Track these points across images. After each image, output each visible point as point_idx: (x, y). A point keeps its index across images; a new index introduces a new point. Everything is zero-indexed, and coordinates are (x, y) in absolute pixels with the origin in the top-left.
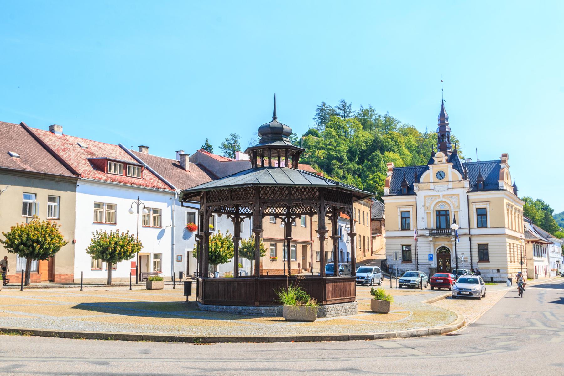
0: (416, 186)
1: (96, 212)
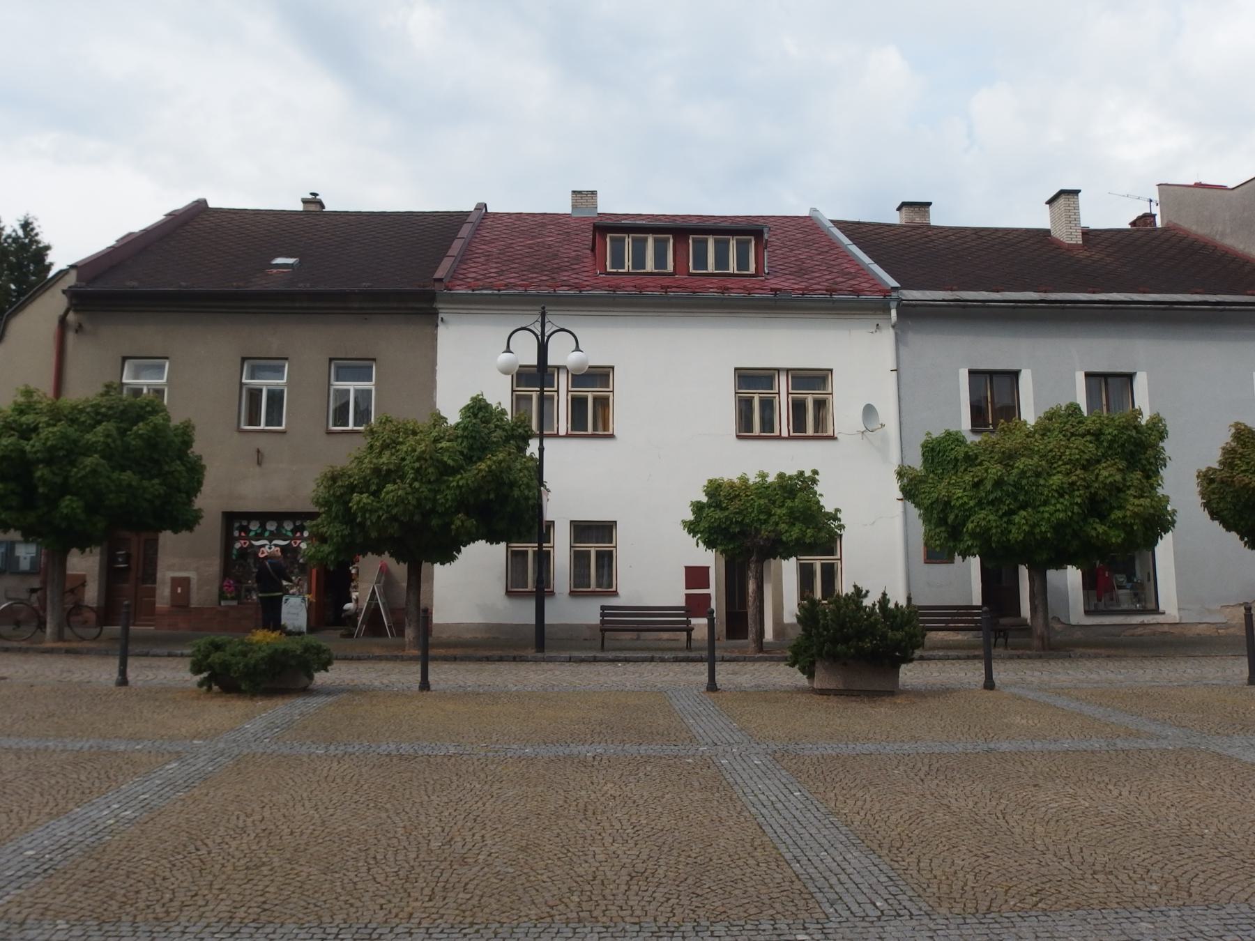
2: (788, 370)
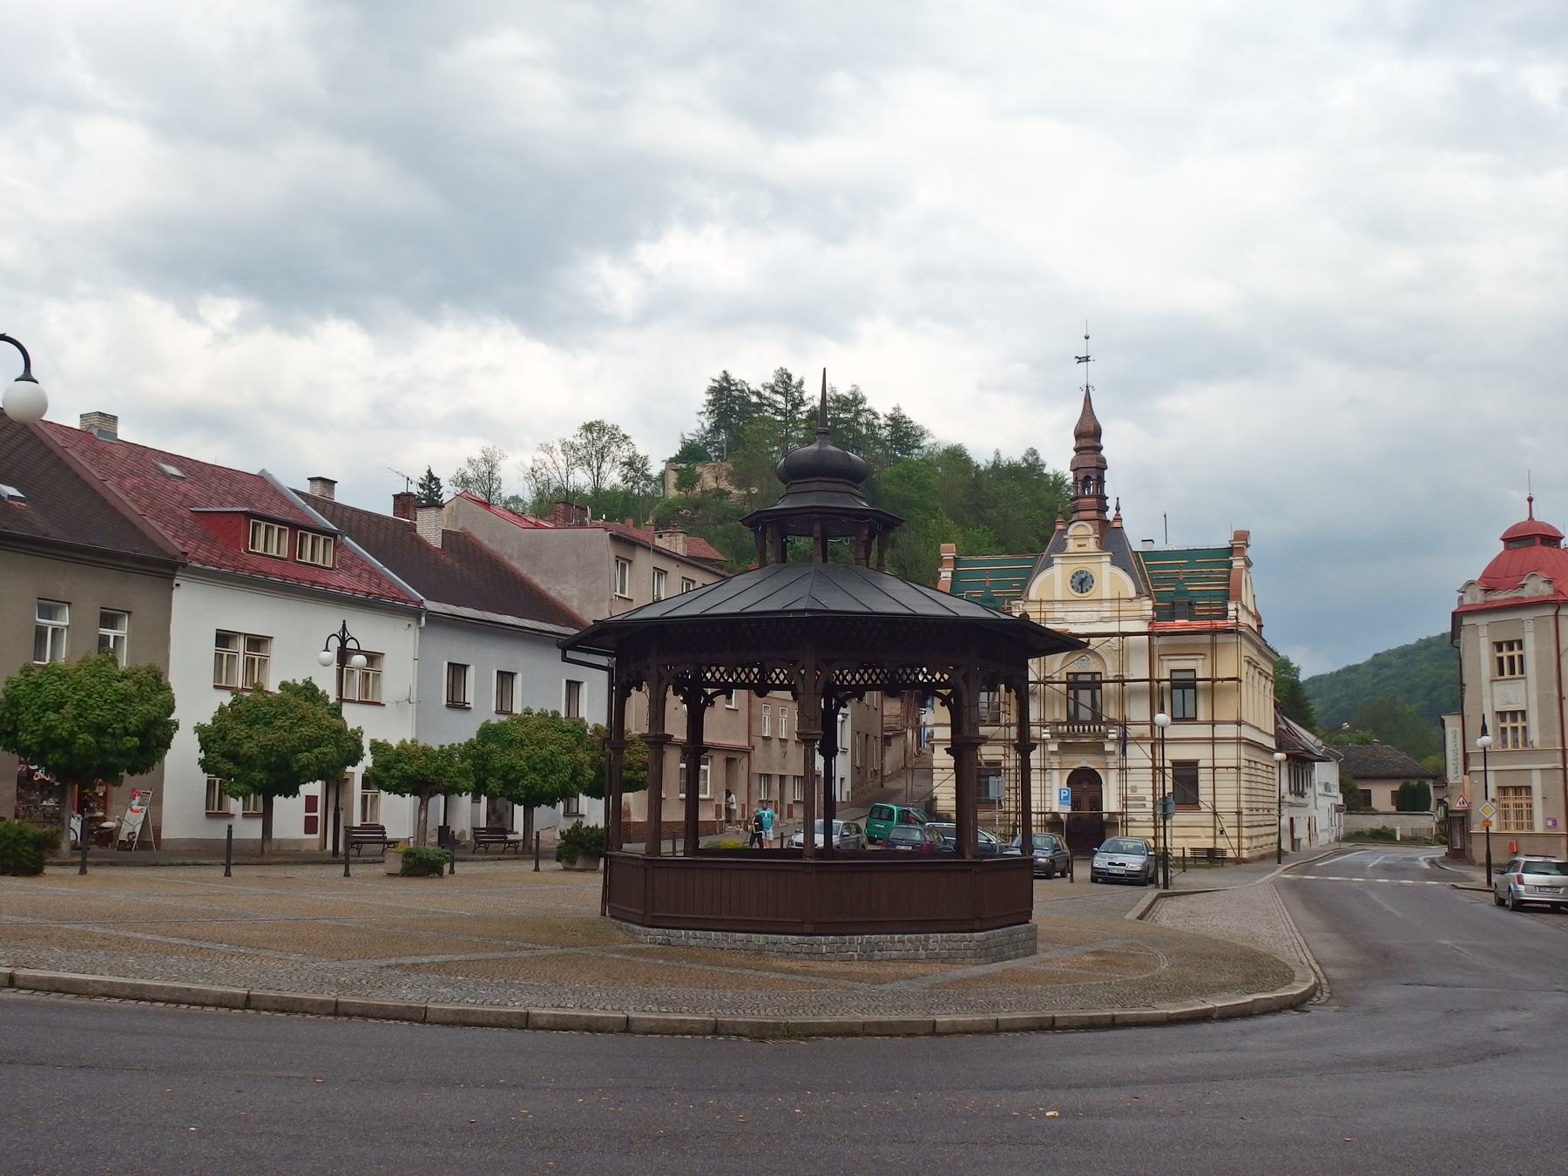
0: (1015, 605)
1: (219, 657)
2: (245, 635)
